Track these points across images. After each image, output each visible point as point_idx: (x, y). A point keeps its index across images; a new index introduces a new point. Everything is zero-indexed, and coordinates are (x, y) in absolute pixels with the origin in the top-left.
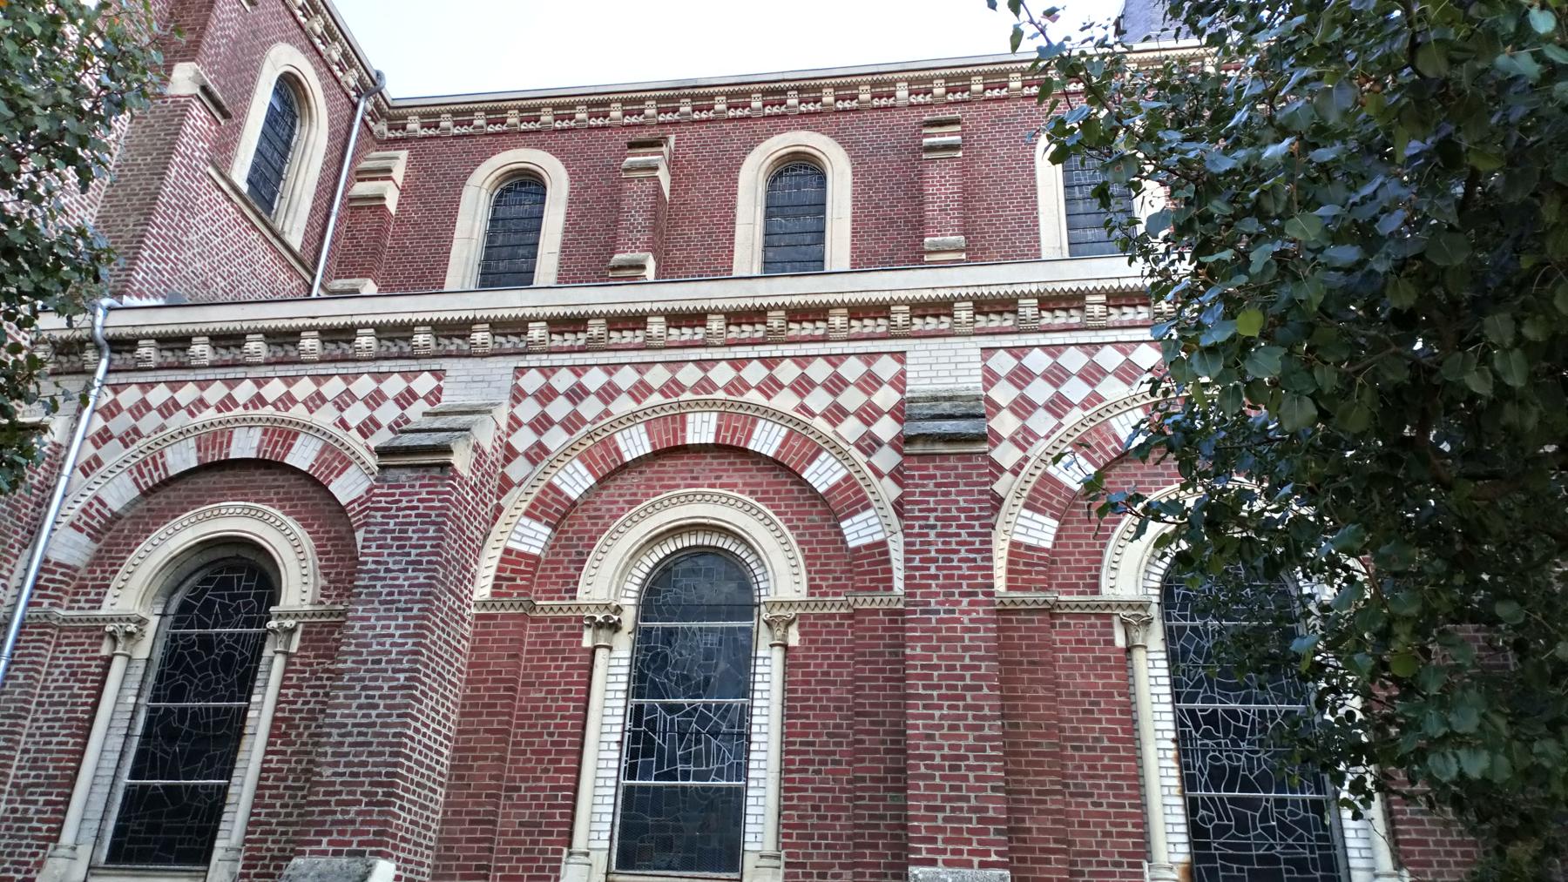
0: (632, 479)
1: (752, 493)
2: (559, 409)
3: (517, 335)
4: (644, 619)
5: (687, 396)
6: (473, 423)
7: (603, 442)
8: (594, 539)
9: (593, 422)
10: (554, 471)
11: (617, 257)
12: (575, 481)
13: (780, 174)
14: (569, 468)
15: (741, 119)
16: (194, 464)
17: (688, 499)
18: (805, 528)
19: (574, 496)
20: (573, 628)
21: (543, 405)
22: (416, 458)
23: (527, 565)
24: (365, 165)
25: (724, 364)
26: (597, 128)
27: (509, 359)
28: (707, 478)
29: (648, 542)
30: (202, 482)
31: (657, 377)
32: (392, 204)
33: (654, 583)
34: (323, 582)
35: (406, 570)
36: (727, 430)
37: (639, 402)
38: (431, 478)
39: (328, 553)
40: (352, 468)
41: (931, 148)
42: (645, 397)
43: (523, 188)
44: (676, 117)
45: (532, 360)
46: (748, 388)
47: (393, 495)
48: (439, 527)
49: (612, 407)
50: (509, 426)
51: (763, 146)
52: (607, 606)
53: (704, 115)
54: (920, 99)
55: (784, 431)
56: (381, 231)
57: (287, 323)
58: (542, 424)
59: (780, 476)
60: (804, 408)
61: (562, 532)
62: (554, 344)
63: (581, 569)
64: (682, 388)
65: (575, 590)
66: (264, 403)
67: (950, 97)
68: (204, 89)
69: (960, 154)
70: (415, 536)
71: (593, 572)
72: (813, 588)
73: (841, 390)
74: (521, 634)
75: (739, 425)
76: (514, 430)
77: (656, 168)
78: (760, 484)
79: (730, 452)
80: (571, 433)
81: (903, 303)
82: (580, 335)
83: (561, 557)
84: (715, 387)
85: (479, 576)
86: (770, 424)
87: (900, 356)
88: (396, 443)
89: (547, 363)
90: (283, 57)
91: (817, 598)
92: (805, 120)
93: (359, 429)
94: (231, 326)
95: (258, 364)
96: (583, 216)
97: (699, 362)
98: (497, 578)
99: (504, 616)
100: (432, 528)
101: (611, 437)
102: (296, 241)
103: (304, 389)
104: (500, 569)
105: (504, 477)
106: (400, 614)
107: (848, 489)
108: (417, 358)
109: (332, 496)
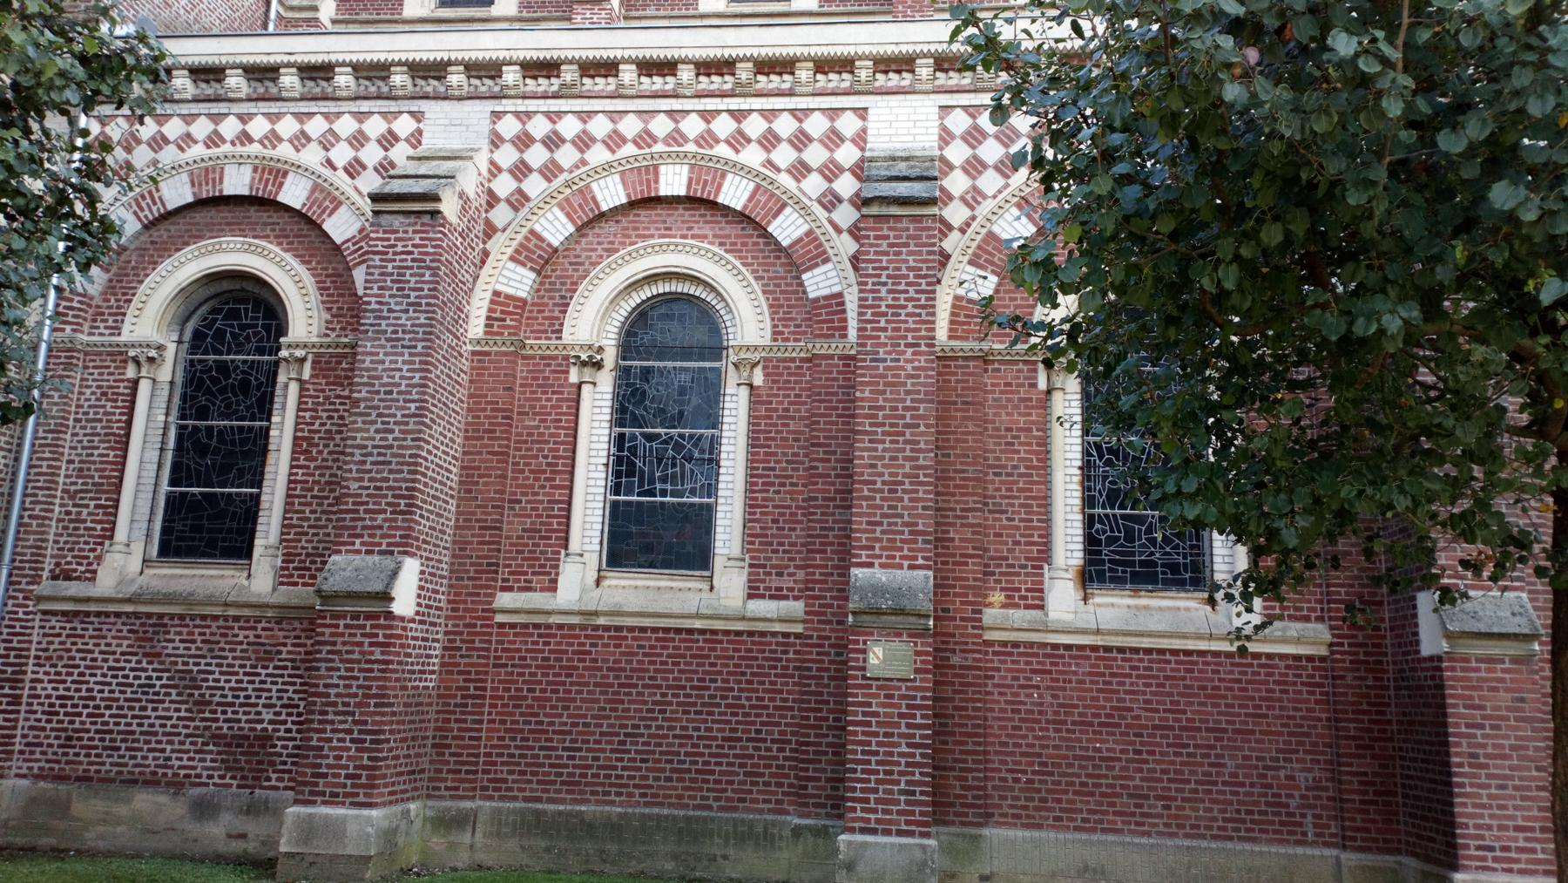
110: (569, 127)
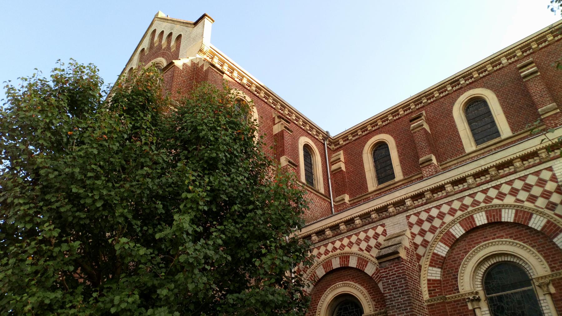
0: (462, 244)
1: (511, 237)
2: (426, 226)
3: (403, 205)
4: (488, 294)
5: (470, 209)
6: (401, 240)
7: (446, 233)
8: (457, 269)
9: (440, 228)
10: (433, 248)
11: (420, 159)
12: (442, 250)
13: (468, 108)
14: (438, 246)
15: (446, 96)
16: (324, 273)
17: (487, 246)
18: (538, 245)
19: (444, 255)
20: (463, 303)
21: (420, 226)
22: (388, 258)
23: (437, 284)
24: (332, 160)
26: (397, 119)
27: (403, 214)
28: (491, 236)
29: (478, 265)
30: (328, 278)
31: (456, 205)
32: (344, 169)
33: (486, 280)
34: (374, 303)
35: (400, 296)
36: (491, 217)
37: (453, 216)
38: (396, 263)
39: (372, 293)
40: (369, 264)
41: (526, 76)
42: (455, 213)
43: (380, 149)
44: (422, 105)
45: (411, 212)
46: (492, 199)
47: (386, 271)
48: (405, 279)
49: (445, 220)
50: (412, 236)
51: (458, 101)
52: (472, 293)
53: (432, 100)
54: (513, 60)
55: (514, 211)
56: (343, 178)
57: (334, 223)
58: (422, 233)
59: (519, 228)
60: (518, 200)
61: (445, 269)
62: (416, 204)
63: (457, 281)
64: (468, 206)
65: (458, 289)
66: (336, 249)
67: (525, 54)
68: (289, 162)
69: (539, 74)
70: (399, 284)
71: (462, 281)
72: (552, 268)
73: (531, 189)
74: (445, 309)
75: (495, 213)
76: (414, 237)
77: (423, 125)
78: (512, 233)
79: (495, 225)
80: (434, 233)
81: (542, 149)
82: (423, 199)
83: (448, 278)
84: (480, 203)
85: (423, 291)
86: (507, 210)
87: (550, 169)
88: (381, 254)
89: (416, 212)
90: (303, 140)
91: (556, 272)
92: (470, 86)
93: (366, 250)
94: (320, 228)
95: (331, 238)
96: (403, 149)
97: (470, 195)
98: (429, 291)
99: (437, 304)
100: (403, 280)
101: (448, 231)
102: (322, 191)
103: (346, 242)
104: (429, 287)
105: (417, 255)
106: (404, 311)
107: (550, 226)
108: (375, 222)
109: (366, 274)
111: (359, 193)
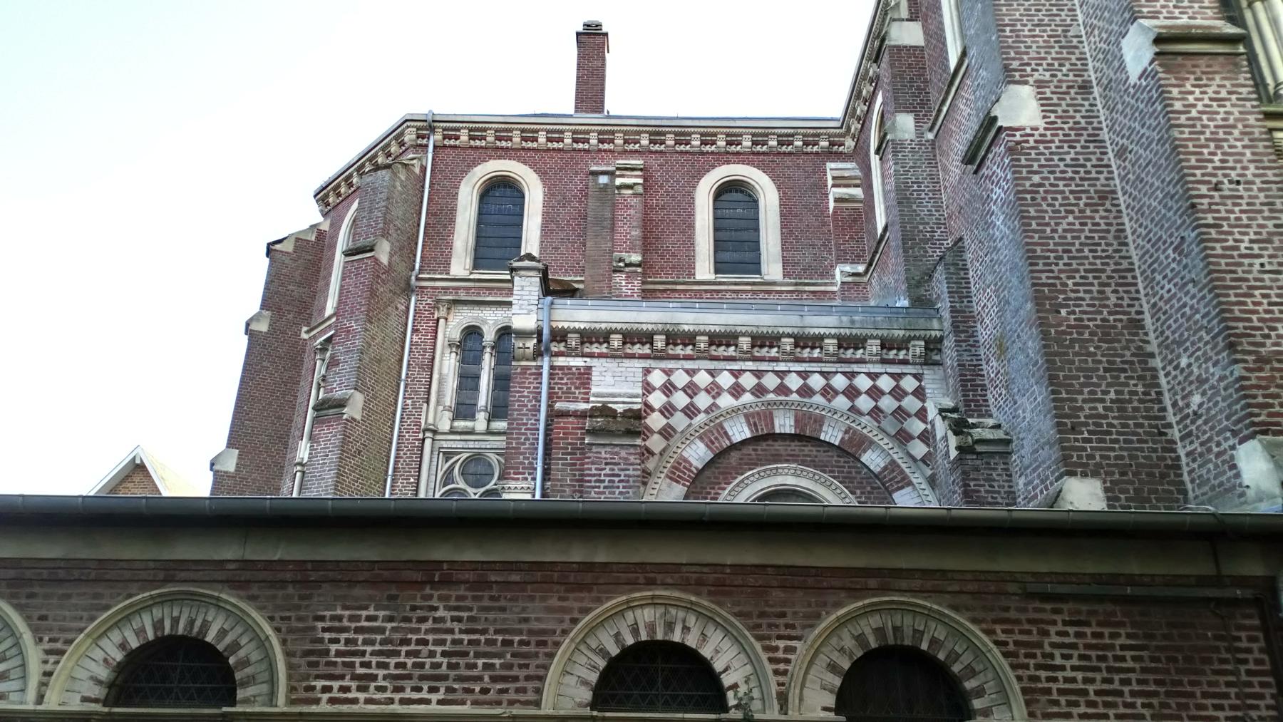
25: (886, 376)
26: (450, 146)
60: (853, 409)
79: (805, 441)
110: (703, 379)
111: (660, 272)
